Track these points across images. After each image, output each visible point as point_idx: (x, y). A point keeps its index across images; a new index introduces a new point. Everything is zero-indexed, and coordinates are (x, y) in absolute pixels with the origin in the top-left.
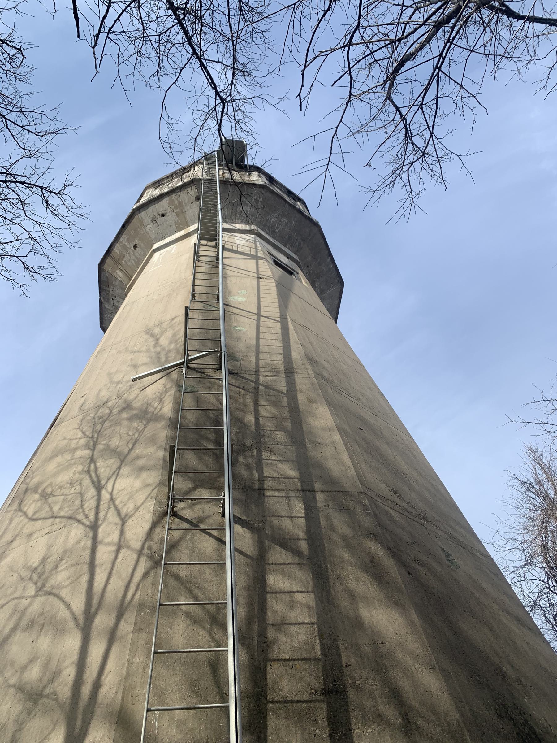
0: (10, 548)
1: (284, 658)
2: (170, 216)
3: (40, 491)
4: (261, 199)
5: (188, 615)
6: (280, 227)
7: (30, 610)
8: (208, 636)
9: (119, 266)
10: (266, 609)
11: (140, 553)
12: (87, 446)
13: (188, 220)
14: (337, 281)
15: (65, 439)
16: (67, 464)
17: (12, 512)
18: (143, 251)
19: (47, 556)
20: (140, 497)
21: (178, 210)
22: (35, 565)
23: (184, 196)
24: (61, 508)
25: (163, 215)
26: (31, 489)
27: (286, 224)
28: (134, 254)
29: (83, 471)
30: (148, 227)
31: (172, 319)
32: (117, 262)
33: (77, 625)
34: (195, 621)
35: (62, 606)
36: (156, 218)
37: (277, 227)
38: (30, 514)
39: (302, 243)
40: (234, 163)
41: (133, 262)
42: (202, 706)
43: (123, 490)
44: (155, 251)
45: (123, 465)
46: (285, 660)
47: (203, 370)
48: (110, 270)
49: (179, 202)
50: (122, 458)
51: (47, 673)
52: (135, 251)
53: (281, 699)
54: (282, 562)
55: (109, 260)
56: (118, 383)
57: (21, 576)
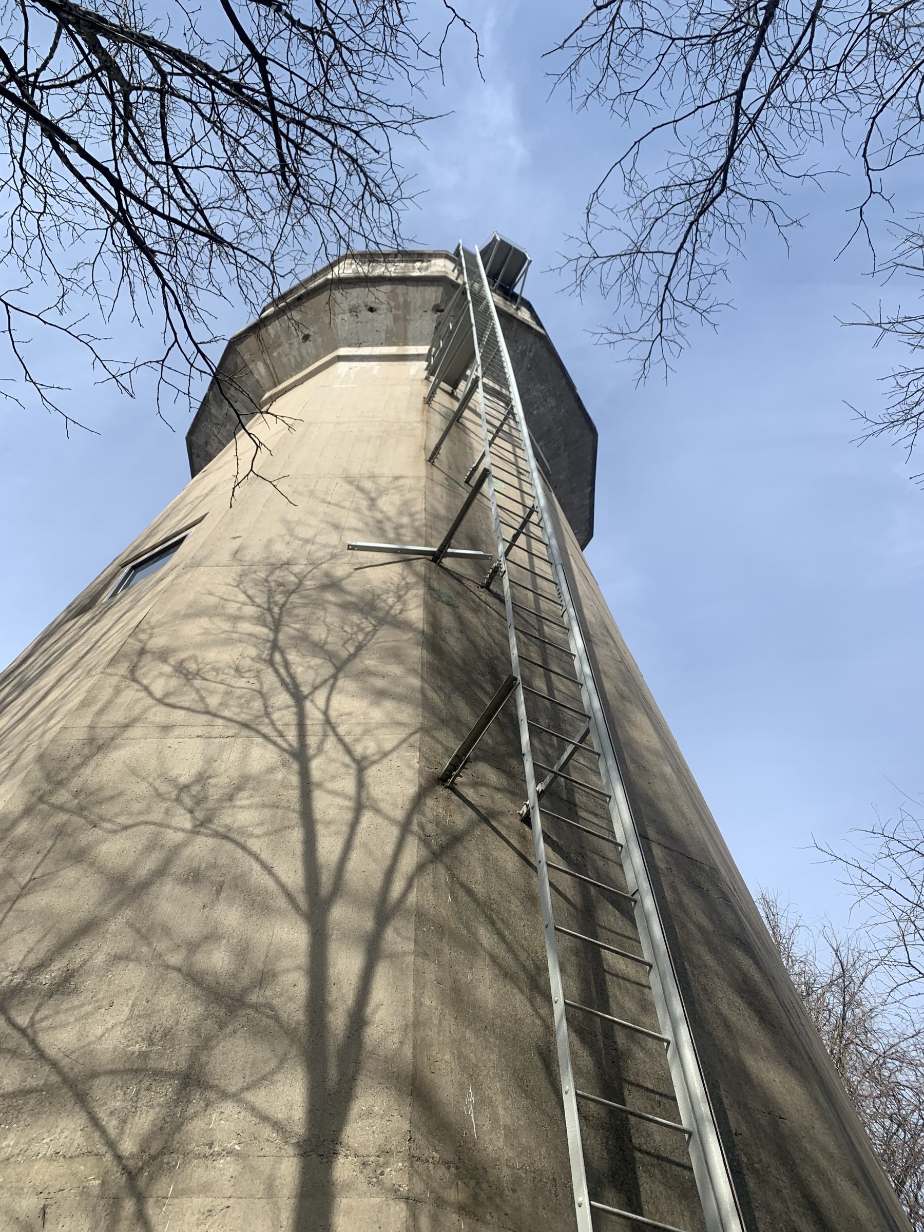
0: (125, 735)
1: (645, 1085)
2: (383, 316)
3: (172, 661)
4: (531, 355)
5: (494, 959)
6: (542, 409)
7: (187, 852)
8: (528, 1005)
9: (265, 356)
10: (608, 997)
11: (405, 828)
12: (260, 620)
13: (410, 334)
14: (584, 528)
15: (211, 594)
16: (223, 636)
17: (117, 678)
18: (318, 349)
19: (207, 774)
20: (390, 739)
21: (400, 312)
22: (183, 780)
23: (415, 294)
24: (223, 704)
25: (371, 310)
26: (153, 653)
27: (552, 408)
28: (299, 350)
29: (259, 658)
30: (340, 317)
31: (397, 478)
32: (265, 349)
33: (297, 908)
34: (506, 975)
35: (256, 866)
36: (360, 308)
37: (538, 408)
38: (159, 693)
39: (563, 448)
40: (498, 281)
41: (293, 360)
42: (651, 1117)
43: (350, 714)
44: (340, 358)
45: (341, 675)
46: (647, 1089)
47: (460, 578)
48: (247, 357)
49: (406, 301)
50: (338, 664)
51: (246, 968)
52: (304, 345)
53: (653, 1151)
54: (618, 931)
55: (251, 340)
56: (307, 541)
57: (156, 790)
